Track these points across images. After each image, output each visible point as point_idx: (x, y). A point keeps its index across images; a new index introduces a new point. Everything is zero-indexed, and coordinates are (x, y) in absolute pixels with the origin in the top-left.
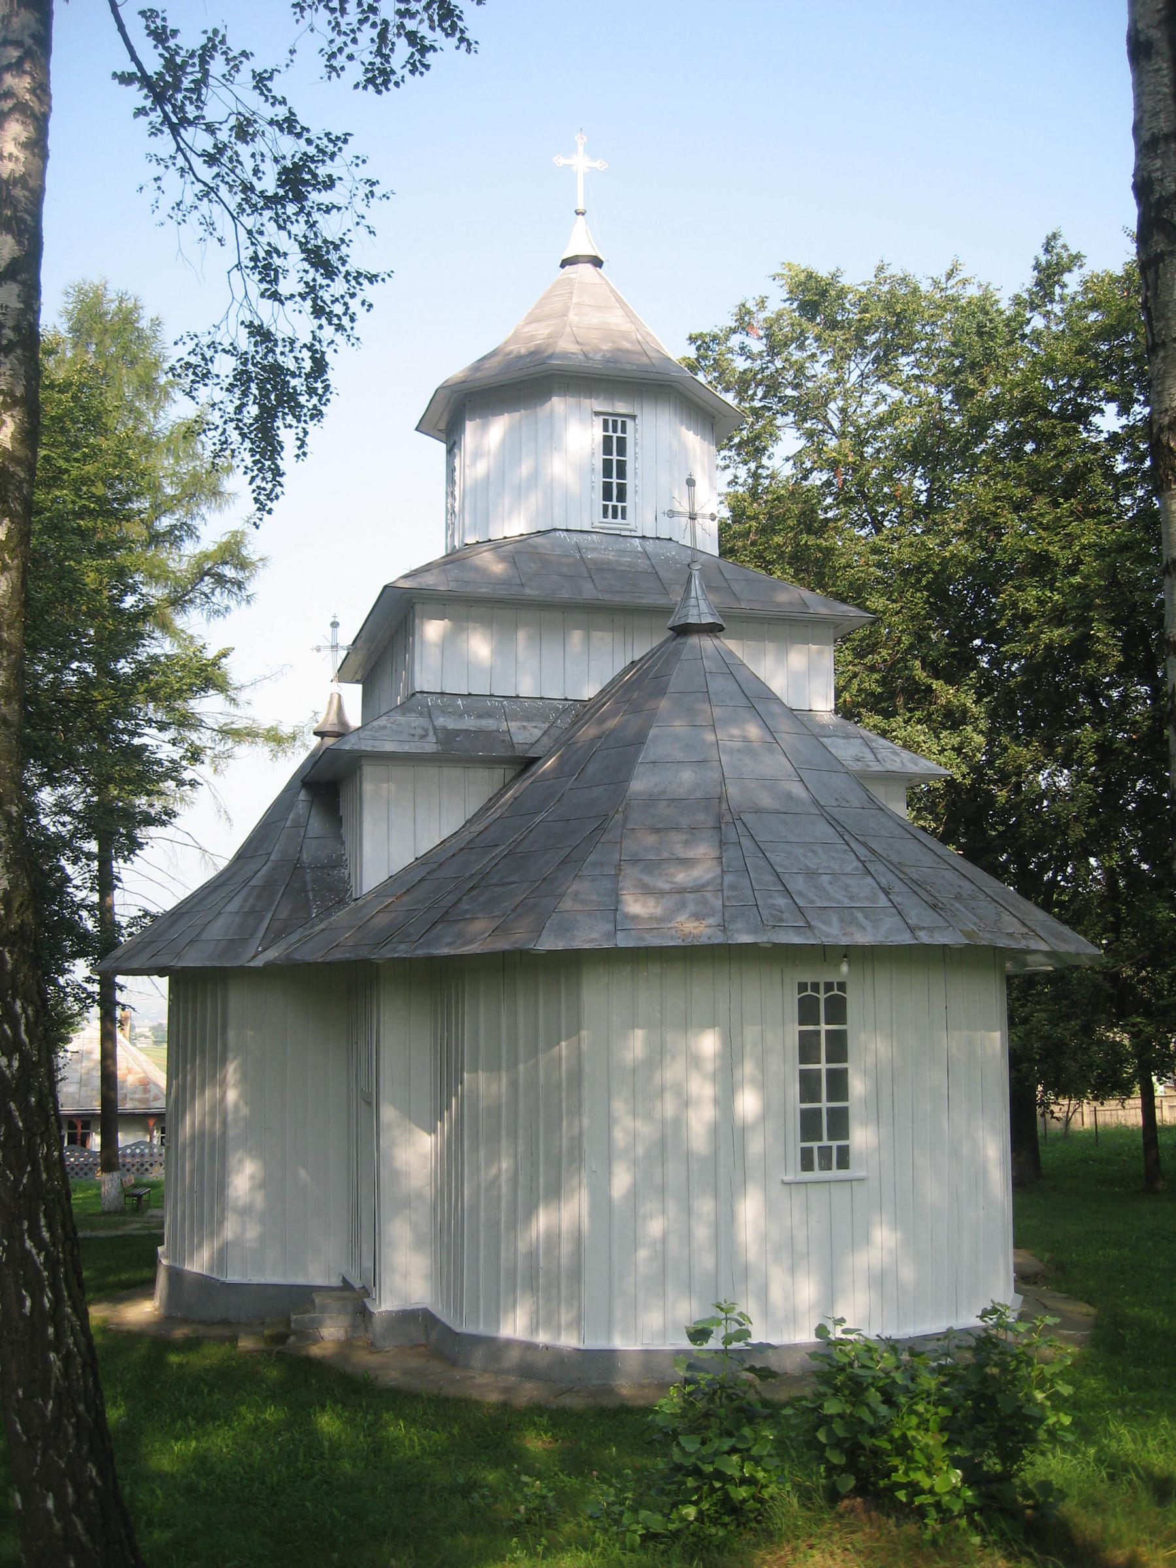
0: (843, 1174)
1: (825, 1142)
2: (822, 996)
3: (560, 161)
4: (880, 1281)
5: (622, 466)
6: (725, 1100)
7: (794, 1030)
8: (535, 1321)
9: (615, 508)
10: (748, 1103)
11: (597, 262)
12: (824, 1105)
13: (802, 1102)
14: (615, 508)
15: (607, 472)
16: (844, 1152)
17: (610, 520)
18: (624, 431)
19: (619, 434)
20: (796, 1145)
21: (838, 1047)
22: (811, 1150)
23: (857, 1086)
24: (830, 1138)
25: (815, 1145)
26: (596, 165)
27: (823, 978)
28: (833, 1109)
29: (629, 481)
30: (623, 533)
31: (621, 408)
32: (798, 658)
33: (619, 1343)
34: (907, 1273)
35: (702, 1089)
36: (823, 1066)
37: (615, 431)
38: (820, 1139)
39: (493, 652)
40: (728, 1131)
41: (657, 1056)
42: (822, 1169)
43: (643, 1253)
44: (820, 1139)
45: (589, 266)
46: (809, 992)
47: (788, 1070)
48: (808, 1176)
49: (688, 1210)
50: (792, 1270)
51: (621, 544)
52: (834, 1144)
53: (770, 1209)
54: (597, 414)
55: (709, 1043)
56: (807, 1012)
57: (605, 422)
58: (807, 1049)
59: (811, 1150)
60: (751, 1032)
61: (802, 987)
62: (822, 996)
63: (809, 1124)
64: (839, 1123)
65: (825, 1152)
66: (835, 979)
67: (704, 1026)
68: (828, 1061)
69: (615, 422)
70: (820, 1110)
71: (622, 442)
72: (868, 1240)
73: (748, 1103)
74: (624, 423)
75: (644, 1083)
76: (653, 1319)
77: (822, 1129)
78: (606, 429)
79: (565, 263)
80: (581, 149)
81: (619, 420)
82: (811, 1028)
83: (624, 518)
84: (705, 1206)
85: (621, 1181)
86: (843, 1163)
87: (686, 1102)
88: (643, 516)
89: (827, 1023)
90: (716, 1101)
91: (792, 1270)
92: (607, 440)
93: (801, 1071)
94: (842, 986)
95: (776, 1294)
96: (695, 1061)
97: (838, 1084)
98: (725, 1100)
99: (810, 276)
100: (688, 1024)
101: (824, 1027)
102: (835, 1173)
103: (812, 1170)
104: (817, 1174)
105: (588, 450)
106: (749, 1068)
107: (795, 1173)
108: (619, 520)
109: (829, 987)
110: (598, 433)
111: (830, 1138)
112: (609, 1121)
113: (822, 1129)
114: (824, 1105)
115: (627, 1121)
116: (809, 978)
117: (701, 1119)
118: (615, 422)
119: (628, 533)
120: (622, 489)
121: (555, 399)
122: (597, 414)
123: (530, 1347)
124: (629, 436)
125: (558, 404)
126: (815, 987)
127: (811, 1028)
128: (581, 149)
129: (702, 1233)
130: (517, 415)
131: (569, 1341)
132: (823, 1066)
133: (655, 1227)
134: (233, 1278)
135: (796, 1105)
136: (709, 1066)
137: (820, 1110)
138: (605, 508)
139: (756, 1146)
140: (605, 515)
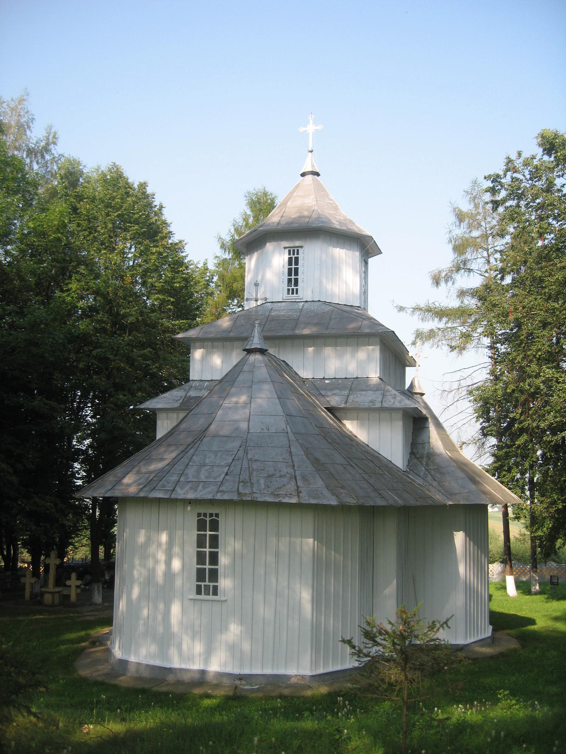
0: (215, 597)
1: (207, 583)
2: (208, 519)
3: (302, 129)
4: (233, 649)
5: (296, 270)
6: (168, 563)
7: (194, 534)
9: (293, 289)
10: (176, 564)
11: (318, 174)
12: (207, 567)
13: (197, 564)
14: (293, 289)
15: (290, 274)
16: (215, 589)
17: (290, 295)
18: (298, 254)
19: (296, 256)
20: (194, 583)
21: (215, 542)
22: (201, 586)
23: (224, 560)
24: (210, 581)
25: (203, 584)
26: (318, 128)
27: (208, 511)
28: (212, 569)
29: (300, 277)
30: (297, 301)
31: (297, 243)
32: (362, 354)
33: (132, 659)
34: (246, 646)
35: (161, 556)
36: (207, 550)
37: (294, 254)
38: (205, 582)
39: (222, 362)
40: (169, 574)
41: (149, 540)
42: (205, 594)
43: (141, 622)
44: (205, 582)
45: (310, 175)
46: (202, 517)
47: (192, 550)
48: (199, 597)
49: (156, 607)
50: (193, 639)
51: (296, 306)
52: (212, 584)
53: (184, 611)
54: (285, 248)
55: (164, 538)
56: (201, 526)
57: (289, 251)
58: (201, 542)
59: (201, 586)
60: (179, 533)
61: (199, 515)
62: (208, 519)
63: (200, 575)
64: (214, 575)
65: (207, 588)
66: (214, 511)
67: (163, 530)
68: (210, 547)
69: (294, 250)
70: (205, 569)
71: (297, 259)
72: (227, 629)
73: (176, 564)
74: (298, 250)
75: (144, 552)
76: (143, 651)
77: (206, 577)
78: (289, 254)
79: (303, 175)
80: (311, 122)
81: (296, 249)
82: (202, 533)
83: (297, 293)
84: (161, 606)
85: (136, 592)
86: (215, 593)
87: (157, 562)
88: (307, 292)
89: (210, 531)
90: (166, 562)
91: (193, 639)
92: (290, 259)
93: (197, 551)
94: (217, 515)
95: (185, 647)
96: (159, 545)
97: (214, 559)
98: (168, 563)
99: (265, 194)
100: (159, 530)
101: (208, 533)
102: (211, 597)
103: (201, 594)
104: (203, 597)
105: (282, 263)
106: (176, 549)
107: (194, 596)
108: (295, 295)
109: (211, 515)
110: (286, 257)
111: (210, 581)
112: (132, 567)
113: (206, 577)
114: (207, 567)
115: (138, 567)
116: (202, 511)
117: (161, 569)
118: (294, 250)
119: (299, 300)
120: (296, 281)
121: (268, 245)
122: (285, 248)
124: (300, 256)
125: (269, 246)
126: (205, 515)
127: (202, 533)
128: (311, 122)
129: (160, 617)
130: (259, 251)
132: (207, 550)
133: (145, 612)
135: (194, 566)
136: (164, 547)
137: (205, 569)
138: (289, 290)
139: (178, 582)
140: (288, 294)
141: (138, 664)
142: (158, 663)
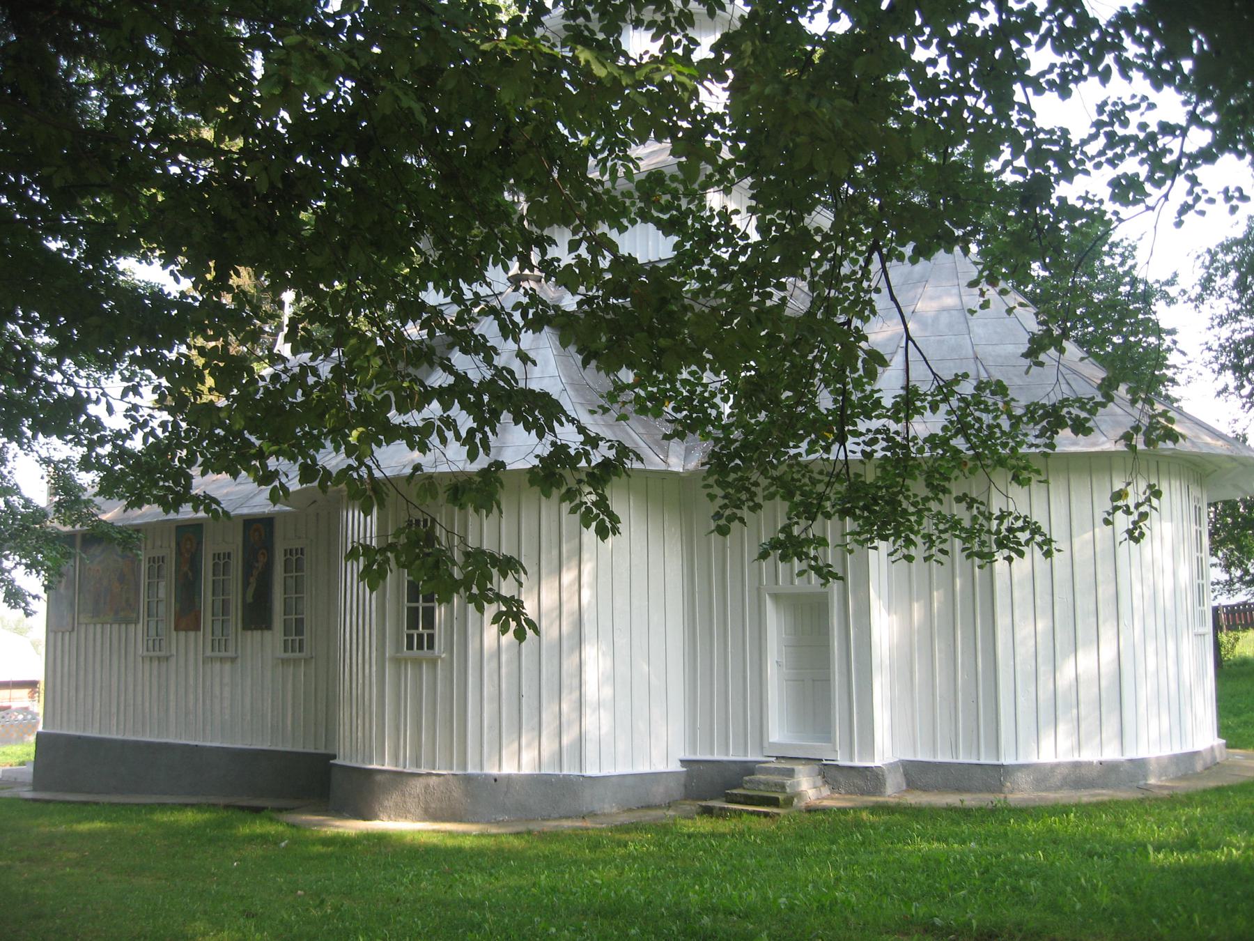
8: (1075, 739)
123: (1077, 765)
131: (1111, 753)
134: (591, 771)
141: (1158, 758)
142: (1177, 750)
